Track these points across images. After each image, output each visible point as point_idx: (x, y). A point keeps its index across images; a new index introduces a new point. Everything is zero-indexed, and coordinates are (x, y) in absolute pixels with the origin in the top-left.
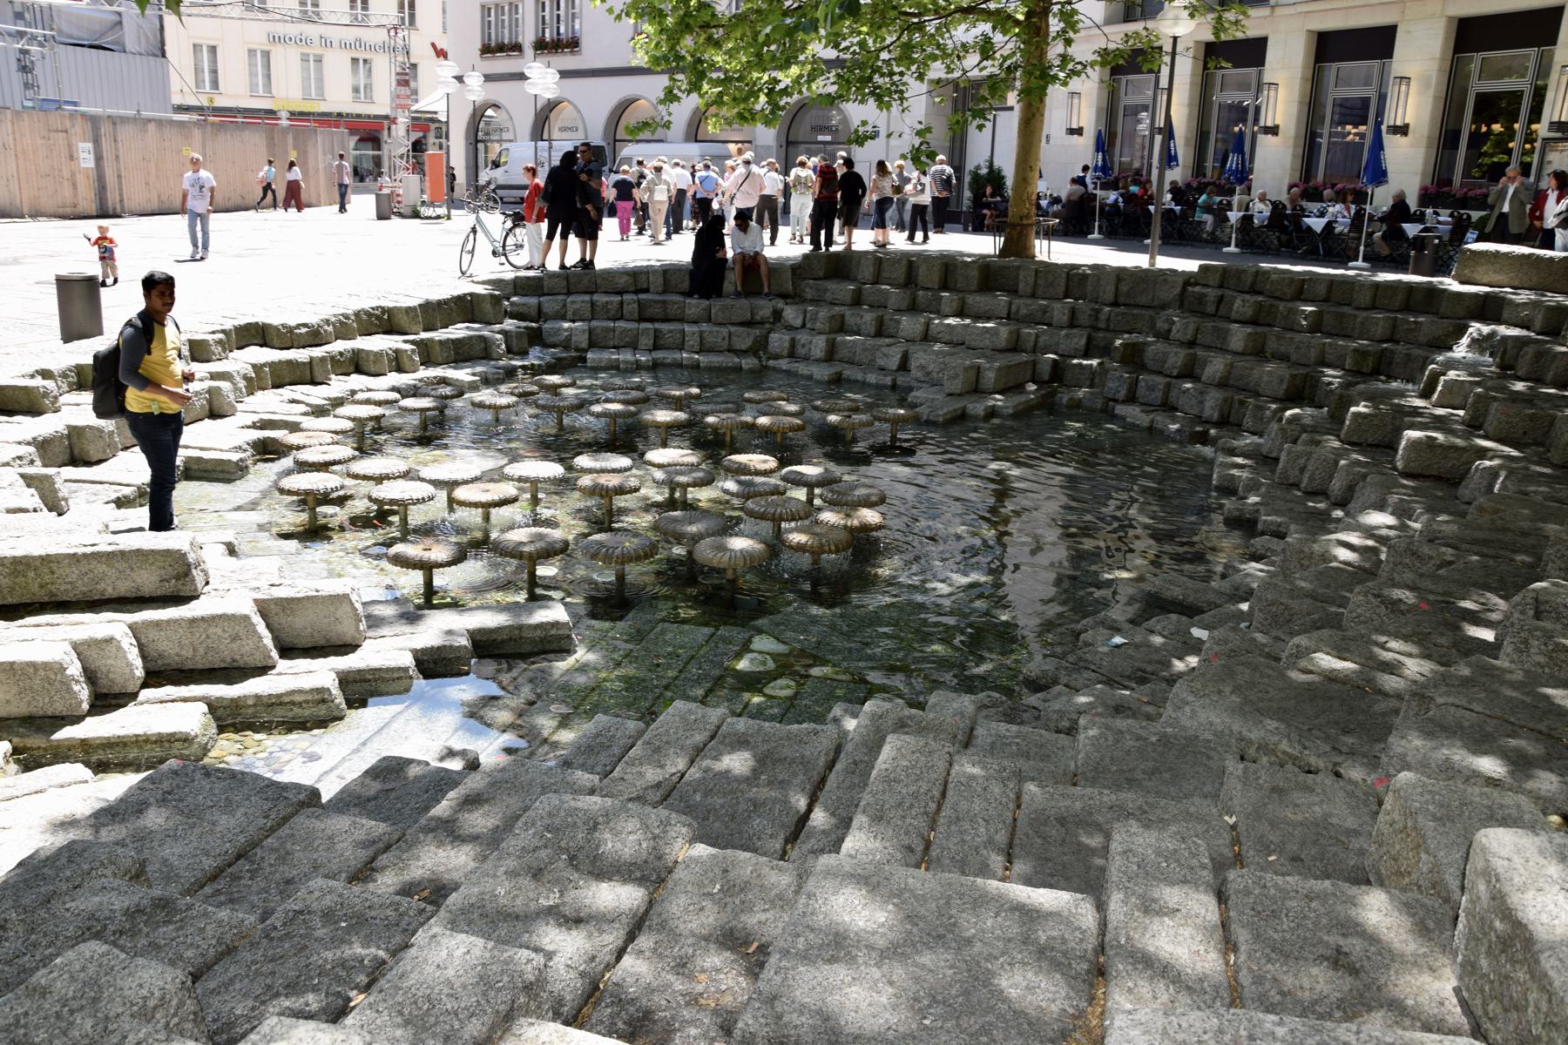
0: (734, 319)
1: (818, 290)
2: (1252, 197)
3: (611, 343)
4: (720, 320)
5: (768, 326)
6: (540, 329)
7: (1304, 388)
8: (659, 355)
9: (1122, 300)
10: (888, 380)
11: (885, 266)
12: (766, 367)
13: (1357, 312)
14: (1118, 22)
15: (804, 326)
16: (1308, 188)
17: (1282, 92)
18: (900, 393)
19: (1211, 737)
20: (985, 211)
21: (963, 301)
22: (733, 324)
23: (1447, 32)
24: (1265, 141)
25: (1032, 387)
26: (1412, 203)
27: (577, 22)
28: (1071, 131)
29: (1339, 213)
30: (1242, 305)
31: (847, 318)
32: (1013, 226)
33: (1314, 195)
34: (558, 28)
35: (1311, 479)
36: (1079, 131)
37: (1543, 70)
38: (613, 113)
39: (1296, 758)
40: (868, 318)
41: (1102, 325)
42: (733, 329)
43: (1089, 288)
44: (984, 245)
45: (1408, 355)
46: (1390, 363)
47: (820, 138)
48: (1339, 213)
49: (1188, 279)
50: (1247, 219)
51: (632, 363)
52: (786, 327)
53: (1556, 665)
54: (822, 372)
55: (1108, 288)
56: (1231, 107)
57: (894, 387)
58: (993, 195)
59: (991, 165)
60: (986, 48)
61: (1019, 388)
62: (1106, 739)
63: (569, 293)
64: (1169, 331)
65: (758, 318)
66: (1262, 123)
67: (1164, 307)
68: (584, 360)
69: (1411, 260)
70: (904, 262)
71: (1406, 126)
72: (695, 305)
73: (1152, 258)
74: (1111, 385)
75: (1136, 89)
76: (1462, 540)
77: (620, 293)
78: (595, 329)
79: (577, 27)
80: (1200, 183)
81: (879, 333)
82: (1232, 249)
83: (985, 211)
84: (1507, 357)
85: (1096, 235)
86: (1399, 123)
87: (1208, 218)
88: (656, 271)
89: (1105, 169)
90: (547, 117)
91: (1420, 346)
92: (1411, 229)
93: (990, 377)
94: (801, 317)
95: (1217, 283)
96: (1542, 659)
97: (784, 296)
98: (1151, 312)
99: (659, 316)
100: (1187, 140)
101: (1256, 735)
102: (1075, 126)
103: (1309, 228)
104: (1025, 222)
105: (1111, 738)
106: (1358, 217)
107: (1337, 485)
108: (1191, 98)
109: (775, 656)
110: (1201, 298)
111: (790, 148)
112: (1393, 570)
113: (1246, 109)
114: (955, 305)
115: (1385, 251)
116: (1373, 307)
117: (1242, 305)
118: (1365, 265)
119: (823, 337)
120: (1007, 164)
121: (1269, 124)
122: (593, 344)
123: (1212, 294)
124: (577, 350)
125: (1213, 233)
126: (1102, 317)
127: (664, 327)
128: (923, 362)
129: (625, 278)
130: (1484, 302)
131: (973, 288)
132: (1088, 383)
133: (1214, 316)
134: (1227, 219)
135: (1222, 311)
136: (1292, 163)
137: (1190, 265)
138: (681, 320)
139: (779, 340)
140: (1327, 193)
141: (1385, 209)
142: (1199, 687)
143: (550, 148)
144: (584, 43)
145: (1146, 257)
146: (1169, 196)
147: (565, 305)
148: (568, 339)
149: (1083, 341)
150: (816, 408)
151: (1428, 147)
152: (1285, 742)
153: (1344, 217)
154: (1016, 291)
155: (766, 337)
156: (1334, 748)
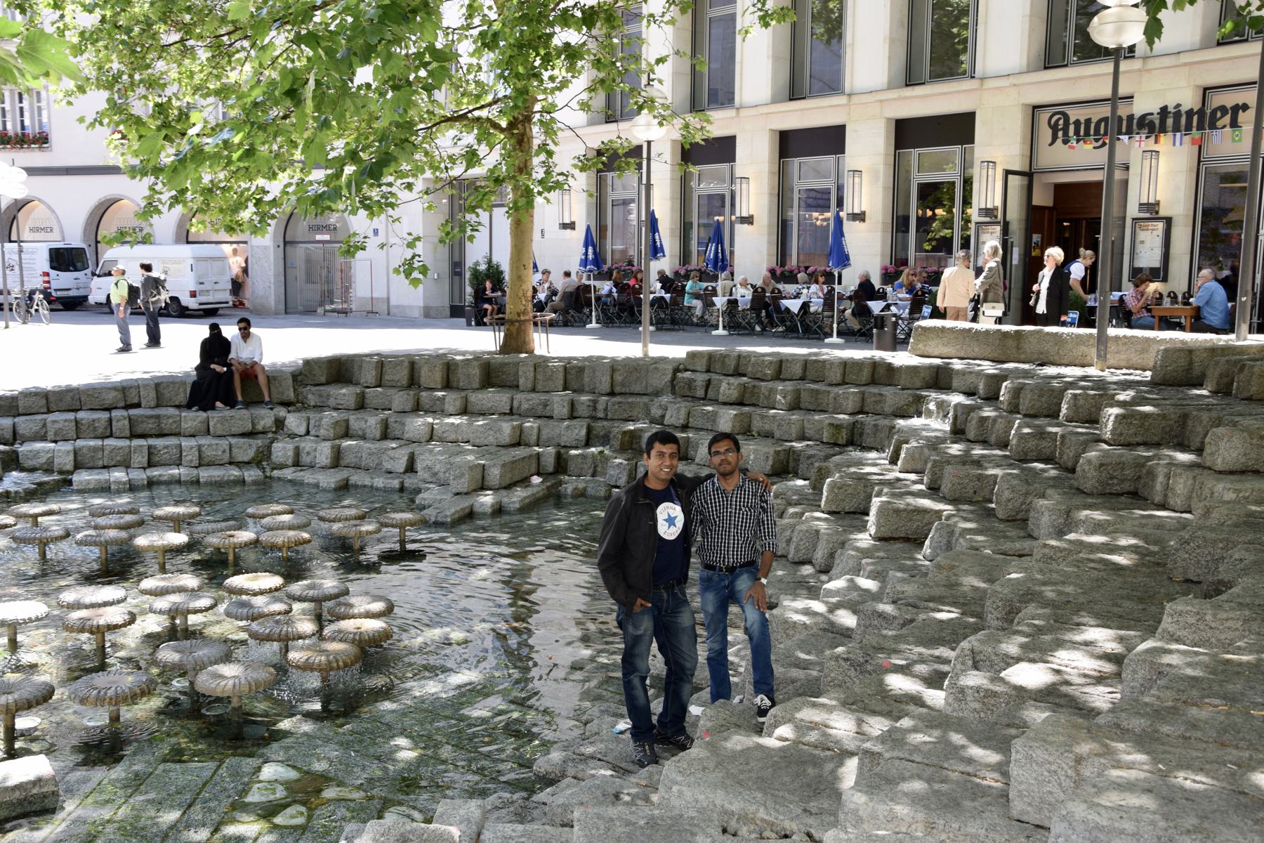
0: (235, 430)
1: (321, 396)
2: (735, 282)
3: (100, 463)
4: (219, 433)
5: (270, 435)
6: (16, 453)
7: (788, 462)
8: (155, 472)
9: (617, 389)
10: (396, 483)
11: (387, 368)
12: (270, 477)
13: (829, 388)
14: (600, 123)
15: (308, 433)
16: (782, 274)
17: (753, 184)
18: (407, 495)
19: (695, 814)
20: (486, 306)
21: (466, 399)
22: (233, 435)
23: (887, 132)
24: (741, 229)
25: (536, 480)
26: (877, 283)
27: (45, 114)
28: (565, 226)
29: (814, 294)
30: (728, 387)
31: (352, 422)
32: (512, 322)
33: (791, 278)
34: (22, 122)
35: (797, 550)
36: (571, 226)
37: (966, 164)
38: (92, 214)
39: (773, 824)
40: (371, 422)
41: (601, 415)
42: (233, 441)
43: (586, 379)
44: (485, 341)
45: (875, 426)
46: (861, 435)
47: (319, 237)
48: (814, 294)
49: (679, 367)
50: (733, 303)
51: (124, 483)
52: (289, 436)
53: (988, 709)
54: (329, 479)
55: (603, 379)
56: (710, 197)
57: (402, 489)
58: (493, 290)
59: (490, 262)
60: (472, 157)
61: (524, 481)
62: (598, 829)
63: (49, 412)
64: (663, 416)
65: (259, 427)
66: (738, 214)
67: (657, 394)
68: (70, 483)
69: (875, 337)
70: (406, 364)
71: (863, 213)
72: (193, 418)
73: (645, 346)
74: (612, 473)
75: (624, 184)
76: (920, 599)
77: (108, 409)
78: (80, 449)
79: (45, 120)
80: (687, 271)
81: (385, 436)
82: (721, 331)
83: (486, 306)
84: (959, 422)
85: (594, 325)
86: (857, 211)
87: (698, 304)
88: (146, 386)
89: (598, 260)
90: (14, 218)
91: (886, 416)
92: (876, 306)
93: (495, 474)
94: (305, 425)
95: (704, 368)
96: (977, 706)
97: (286, 404)
98: (646, 399)
99: (153, 432)
100: (672, 230)
101: (736, 806)
102: (567, 221)
103: (787, 310)
104: (522, 318)
105: (603, 827)
106: (829, 300)
107: (820, 555)
108: (672, 192)
109: (288, 785)
110: (690, 383)
111: (288, 248)
112: (865, 632)
113: (722, 197)
114: (458, 404)
115: (856, 327)
116: (843, 383)
117: (728, 387)
118: (840, 341)
119: (328, 444)
120: (503, 259)
121: (745, 214)
122: (78, 466)
123: (701, 378)
124: (61, 472)
125: (702, 317)
126: (600, 407)
127: (159, 442)
128: (429, 463)
129: (113, 394)
130: (937, 373)
131: (476, 385)
132: (591, 471)
133: (703, 399)
134: (713, 304)
135: (711, 394)
136: (769, 250)
137: (676, 351)
138: (177, 434)
139: (282, 450)
140: (801, 276)
141: (853, 288)
142: (685, 766)
143: (21, 251)
144: (54, 138)
145: (640, 345)
146: (659, 285)
147: (44, 425)
148: (50, 462)
149: (584, 432)
150: (322, 519)
151: (884, 231)
152: (762, 810)
153: (819, 297)
154: (517, 386)
155: (269, 447)
156: (805, 810)
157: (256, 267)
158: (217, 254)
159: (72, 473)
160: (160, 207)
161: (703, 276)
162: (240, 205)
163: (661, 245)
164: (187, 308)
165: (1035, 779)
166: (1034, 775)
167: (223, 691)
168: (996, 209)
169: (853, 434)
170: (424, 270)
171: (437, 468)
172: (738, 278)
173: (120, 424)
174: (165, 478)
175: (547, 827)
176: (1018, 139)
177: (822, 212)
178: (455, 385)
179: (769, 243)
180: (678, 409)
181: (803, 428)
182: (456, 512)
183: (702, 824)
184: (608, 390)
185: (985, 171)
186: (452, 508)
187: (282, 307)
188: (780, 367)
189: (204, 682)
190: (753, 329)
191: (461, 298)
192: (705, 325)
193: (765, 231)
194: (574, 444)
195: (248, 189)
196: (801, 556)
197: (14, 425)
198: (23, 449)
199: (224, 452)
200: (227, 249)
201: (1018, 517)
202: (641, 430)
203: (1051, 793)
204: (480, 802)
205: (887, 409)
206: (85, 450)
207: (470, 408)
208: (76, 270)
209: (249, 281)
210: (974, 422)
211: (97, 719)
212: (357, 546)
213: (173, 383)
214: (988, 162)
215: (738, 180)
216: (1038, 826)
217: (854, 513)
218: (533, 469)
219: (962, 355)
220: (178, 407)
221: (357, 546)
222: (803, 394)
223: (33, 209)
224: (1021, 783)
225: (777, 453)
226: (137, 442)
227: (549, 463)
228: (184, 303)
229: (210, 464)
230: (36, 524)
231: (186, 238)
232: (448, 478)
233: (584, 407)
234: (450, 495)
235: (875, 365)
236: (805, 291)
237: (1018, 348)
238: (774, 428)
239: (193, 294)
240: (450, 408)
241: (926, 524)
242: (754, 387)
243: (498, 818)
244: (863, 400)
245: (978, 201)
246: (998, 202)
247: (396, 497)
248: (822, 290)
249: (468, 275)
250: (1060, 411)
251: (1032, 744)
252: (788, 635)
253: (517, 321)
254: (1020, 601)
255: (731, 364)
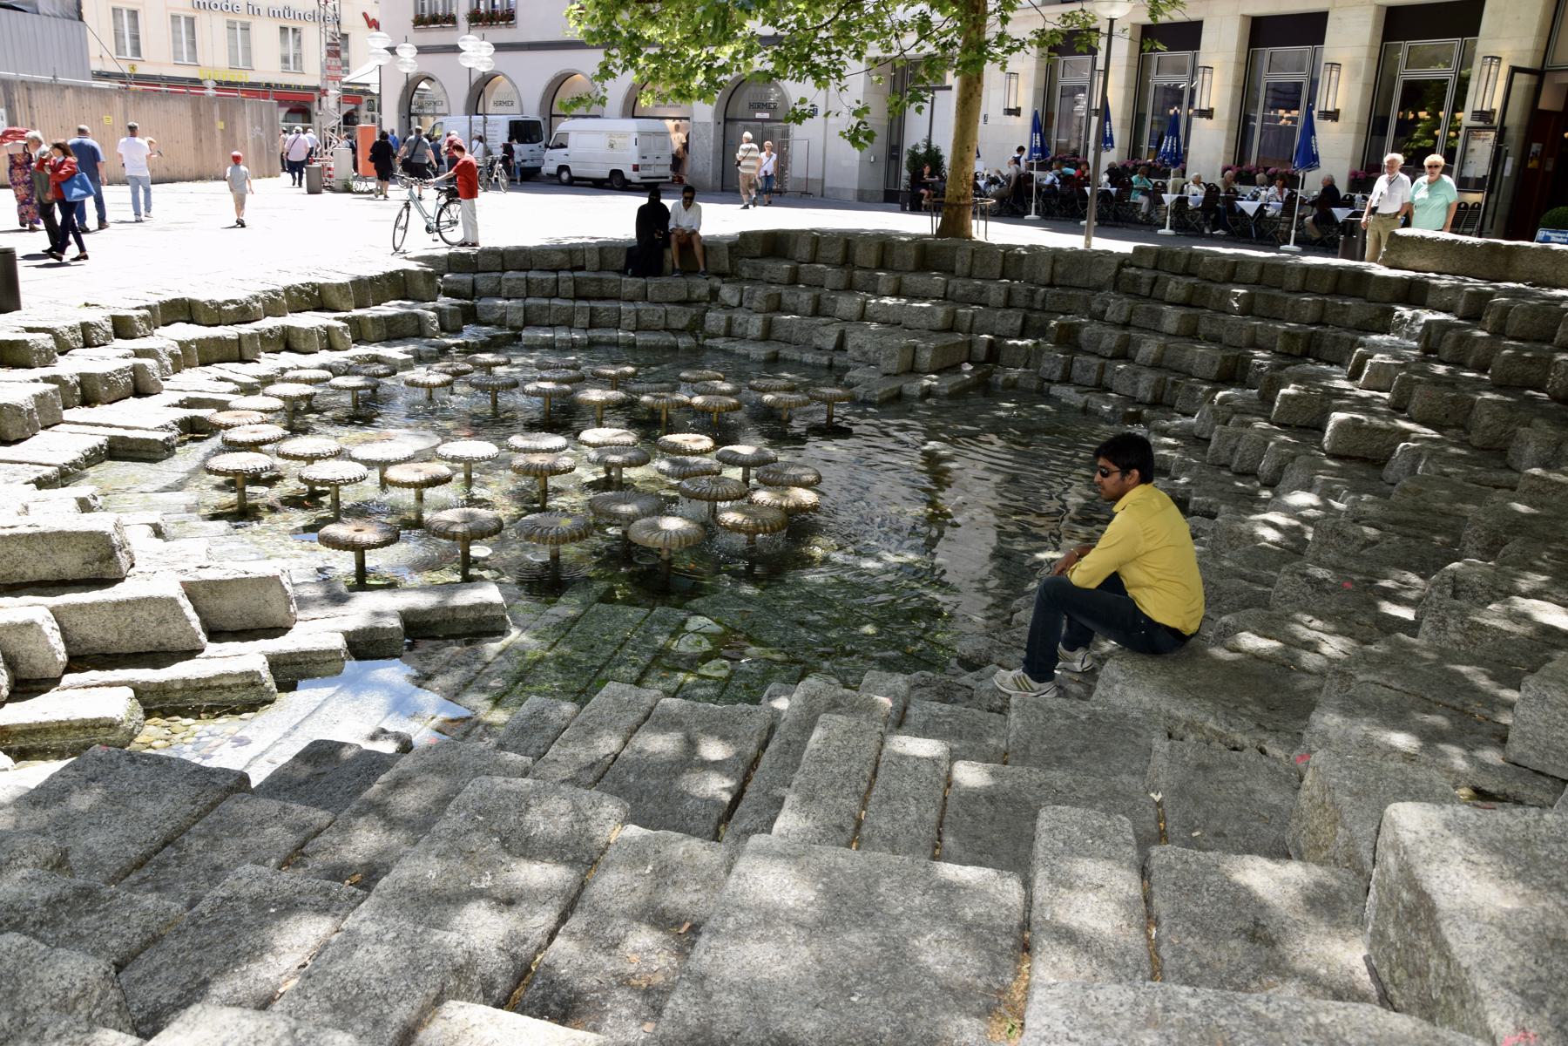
0: (671, 297)
1: (755, 269)
4: (656, 299)
6: (474, 307)
8: (595, 333)
9: (1057, 281)
10: (825, 360)
15: (741, 304)
16: (1241, 172)
18: (835, 372)
20: (923, 191)
22: (670, 303)
23: (1376, 21)
24: (1199, 124)
25: (968, 367)
26: (1343, 189)
28: (1009, 112)
30: (1175, 287)
32: (950, 206)
33: (1247, 178)
35: (1242, 460)
36: (1016, 112)
37: (1466, 60)
38: (542, 103)
39: (1222, 735)
40: (805, 297)
41: (1038, 306)
42: (669, 307)
43: (1025, 269)
44: (921, 225)
46: (1319, 346)
47: (758, 115)
49: (1123, 261)
50: (1182, 201)
51: (568, 342)
52: (722, 306)
53: (1471, 642)
54: (759, 352)
56: (1167, 89)
57: (830, 366)
61: (955, 368)
62: (1037, 718)
64: (1104, 312)
65: (695, 296)
67: (1099, 288)
68: (519, 338)
70: (842, 241)
72: (631, 284)
73: (1088, 239)
74: (1046, 366)
75: (1074, 71)
77: (556, 271)
78: (530, 307)
80: (1136, 165)
81: (816, 312)
82: (1167, 231)
83: (923, 191)
85: (1033, 216)
86: (1330, 108)
87: (1143, 200)
91: (1349, 329)
92: (1341, 214)
94: (738, 296)
95: (1151, 264)
96: (1458, 637)
97: (721, 275)
98: (1087, 293)
99: (595, 294)
100: (1123, 121)
101: (1182, 713)
102: (1012, 106)
103: (1242, 211)
104: (962, 202)
107: (1265, 466)
108: (1128, 81)
111: (728, 125)
113: (1181, 92)
114: (892, 285)
116: (1303, 290)
117: (1175, 287)
118: (1296, 248)
119: (761, 316)
120: (945, 143)
121: (1204, 107)
122: (527, 323)
123: (1147, 275)
125: (1148, 215)
126: (1038, 298)
128: (860, 342)
129: (562, 256)
131: (911, 267)
133: (1148, 297)
134: (1162, 202)
135: (1157, 292)
136: (1227, 146)
137: (1125, 247)
138: (618, 298)
139: (715, 319)
141: (1316, 193)
143: (485, 122)
147: (499, 283)
149: (1019, 322)
150: (752, 388)
151: (1358, 132)
152: (1211, 719)
154: (953, 272)
155: (703, 316)
157: (696, 143)
158: (661, 129)
159: (521, 329)
160: (615, 71)
161: (1151, 171)
162: (690, 72)
163: (1111, 135)
164: (629, 182)
165: (1545, 721)
166: (1544, 717)
167: (654, 543)
168: (1493, 112)
169: (1309, 344)
170: (870, 136)
171: (868, 347)
172: (1191, 174)
173: (566, 285)
174: (604, 339)
175: (975, 711)
176: (1534, 30)
177: (1288, 111)
178: (889, 265)
179: (1228, 139)
180: (1121, 306)
181: (1254, 335)
182: (885, 392)
183: (1148, 727)
184: (1048, 281)
185: (1486, 69)
186: (881, 388)
187: (719, 184)
188: (1235, 269)
189: (640, 533)
190: (1203, 231)
191: (896, 182)
192: (1149, 224)
193: (1225, 125)
194: (1008, 333)
195: (699, 55)
196: (1245, 466)
197: (474, 280)
198: (482, 303)
199: (660, 317)
200: (670, 124)
201: (1497, 446)
202: (1080, 324)
203: (1562, 738)
204: (906, 677)
205: (1350, 322)
206: (534, 309)
207: (903, 290)
208: (532, 142)
209: (689, 158)
210: (1450, 341)
211: (539, 556)
212: (785, 417)
213: (616, 248)
214: (1493, 57)
215: (1201, 70)
216: (1537, 772)
217: (1306, 427)
218: (965, 355)
219: (1441, 269)
220: (618, 272)
221: (785, 417)
222: (1257, 299)
223: (497, 84)
224: (1525, 724)
225: (1225, 359)
226: (579, 303)
227: (981, 352)
228: (627, 176)
229: (647, 329)
230: (490, 373)
231: (631, 109)
232: (878, 359)
233: (1021, 297)
234: (879, 375)
235: (1339, 272)
236: (1263, 193)
237: (1507, 265)
238: (1224, 332)
239: (636, 168)
240: (882, 288)
241: (1389, 445)
242: (1204, 288)
243: (920, 696)
244: (1323, 309)
245: (1473, 102)
246: (1497, 105)
247: (824, 373)
248: (1281, 193)
249: (905, 158)
250: (1555, 335)
251: (1548, 683)
252: (1231, 546)
253: (956, 205)
254: (1506, 533)
255: (1182, 262)
